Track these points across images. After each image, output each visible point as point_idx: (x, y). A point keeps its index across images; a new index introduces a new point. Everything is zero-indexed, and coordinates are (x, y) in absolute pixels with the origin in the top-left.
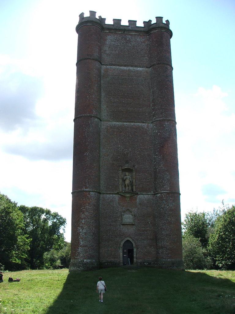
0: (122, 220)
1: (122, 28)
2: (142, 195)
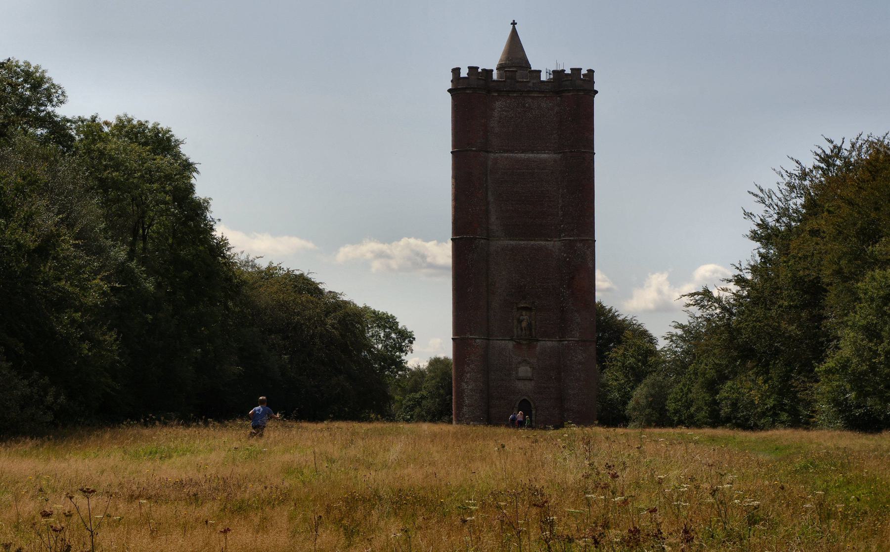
0: (517, 373)
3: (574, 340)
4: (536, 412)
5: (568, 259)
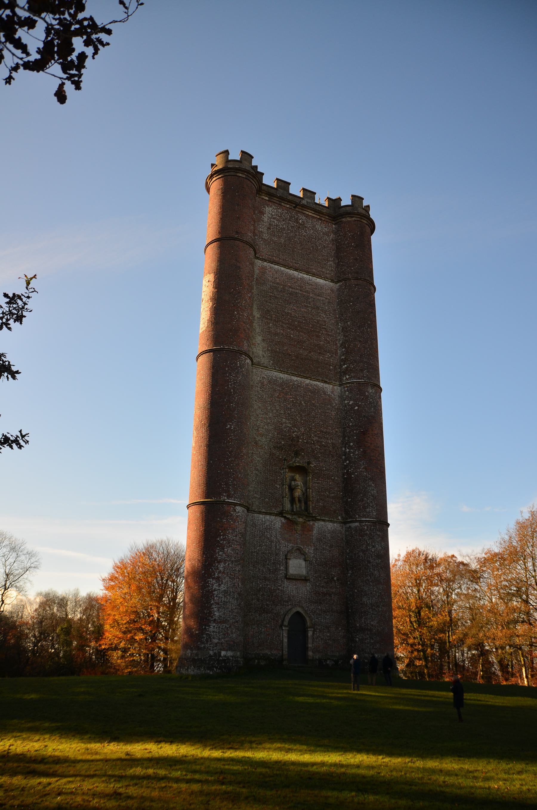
0: (287, 568)
1: (290, 198)
2: (323, 523)
3: (368, 521)
4: (313, 634)
5: (356, 408)
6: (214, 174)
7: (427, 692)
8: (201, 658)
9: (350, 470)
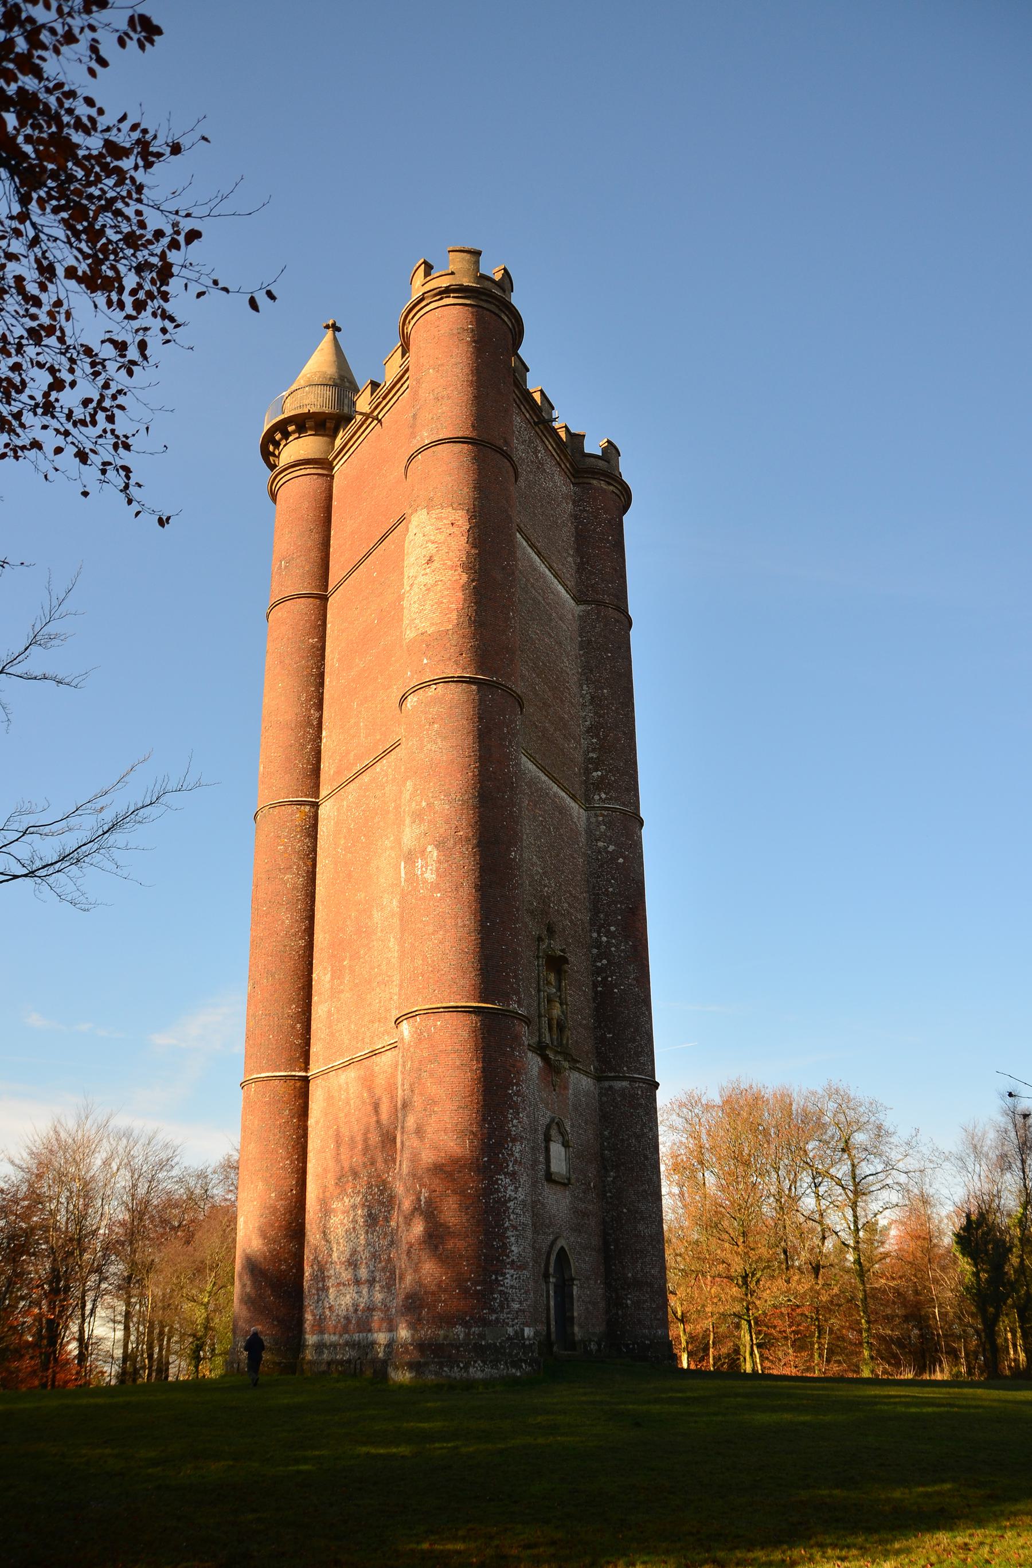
6: (454, 291)
7: (1014, 1393)
8: (495, 1344)
9: (610, 979)
